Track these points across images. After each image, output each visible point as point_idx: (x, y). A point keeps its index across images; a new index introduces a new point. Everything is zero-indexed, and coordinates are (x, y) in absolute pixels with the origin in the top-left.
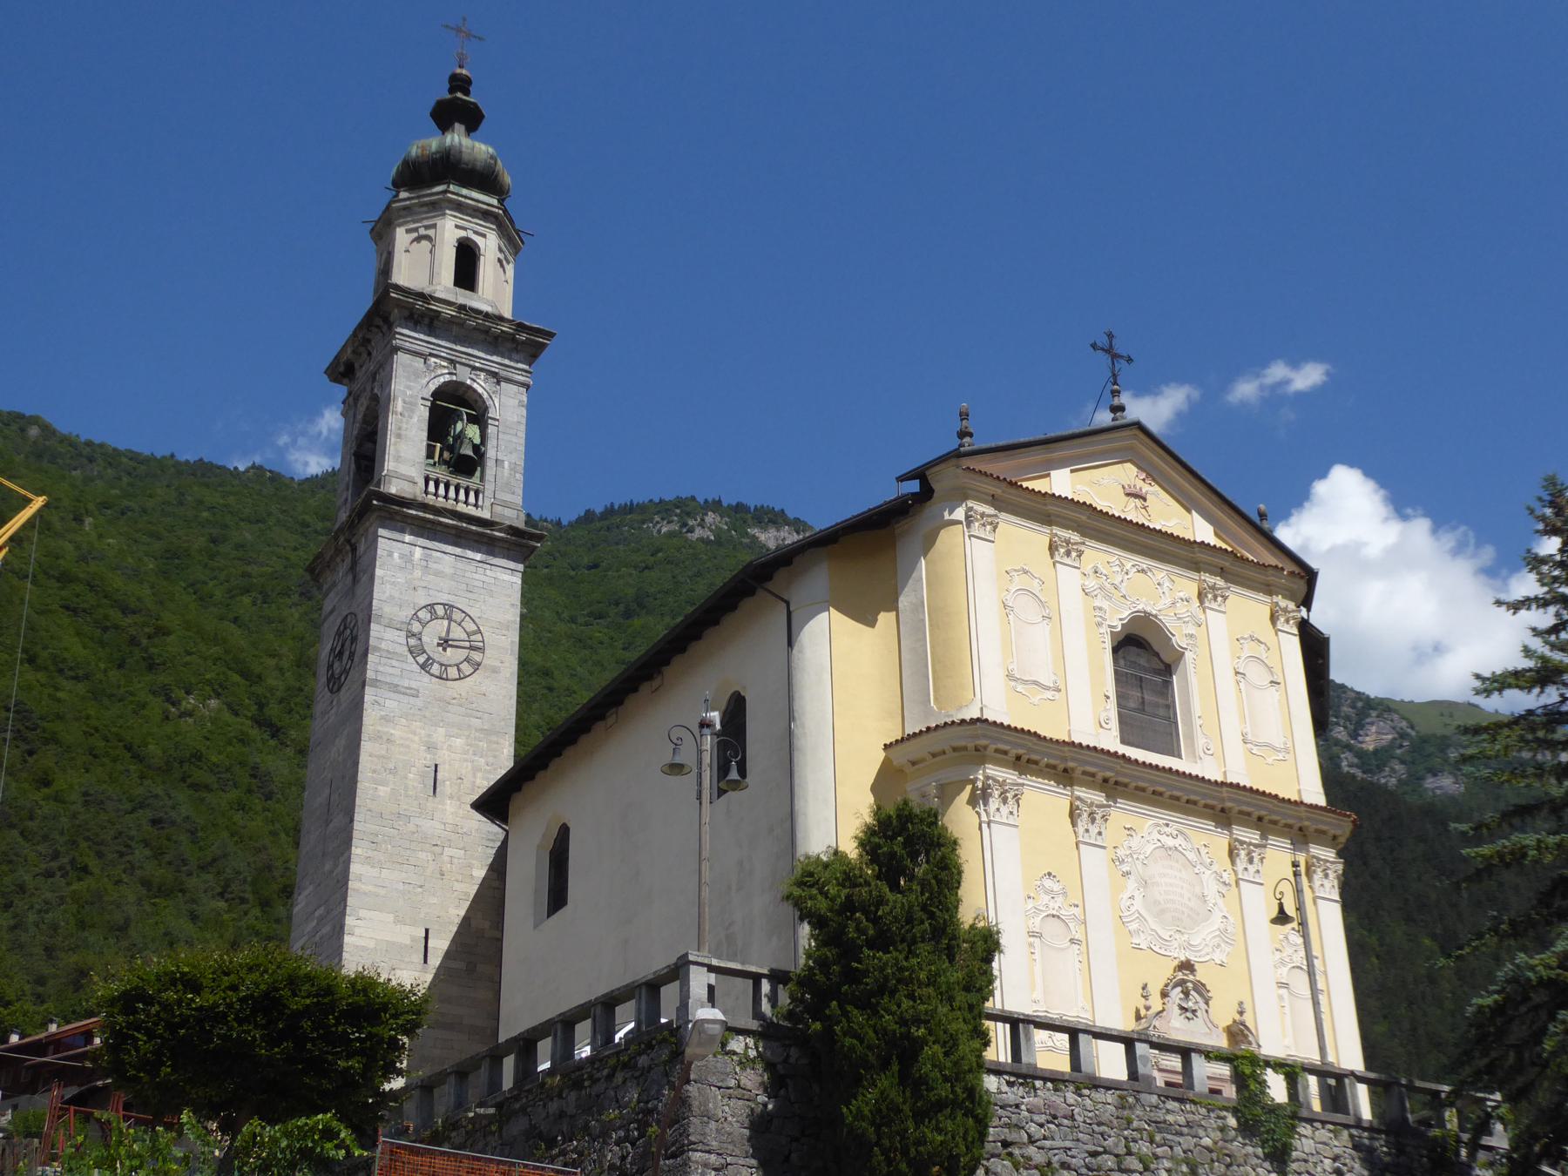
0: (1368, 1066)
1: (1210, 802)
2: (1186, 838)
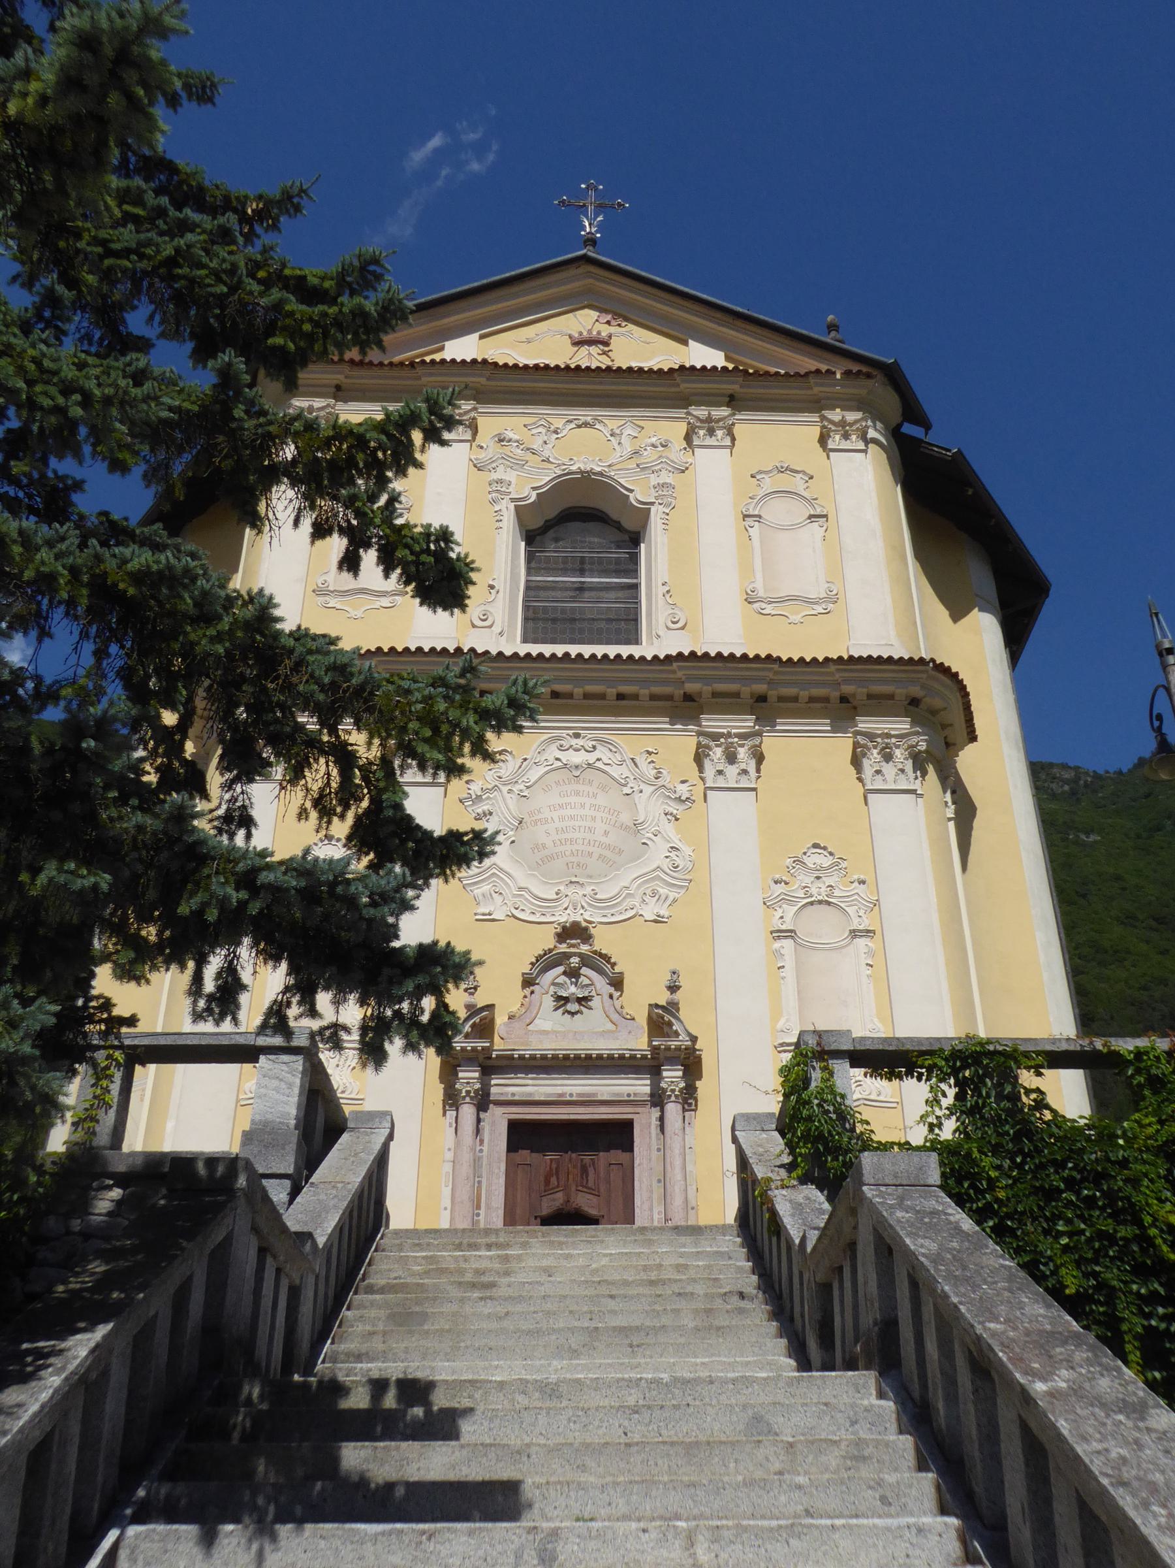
1: (657, 690)
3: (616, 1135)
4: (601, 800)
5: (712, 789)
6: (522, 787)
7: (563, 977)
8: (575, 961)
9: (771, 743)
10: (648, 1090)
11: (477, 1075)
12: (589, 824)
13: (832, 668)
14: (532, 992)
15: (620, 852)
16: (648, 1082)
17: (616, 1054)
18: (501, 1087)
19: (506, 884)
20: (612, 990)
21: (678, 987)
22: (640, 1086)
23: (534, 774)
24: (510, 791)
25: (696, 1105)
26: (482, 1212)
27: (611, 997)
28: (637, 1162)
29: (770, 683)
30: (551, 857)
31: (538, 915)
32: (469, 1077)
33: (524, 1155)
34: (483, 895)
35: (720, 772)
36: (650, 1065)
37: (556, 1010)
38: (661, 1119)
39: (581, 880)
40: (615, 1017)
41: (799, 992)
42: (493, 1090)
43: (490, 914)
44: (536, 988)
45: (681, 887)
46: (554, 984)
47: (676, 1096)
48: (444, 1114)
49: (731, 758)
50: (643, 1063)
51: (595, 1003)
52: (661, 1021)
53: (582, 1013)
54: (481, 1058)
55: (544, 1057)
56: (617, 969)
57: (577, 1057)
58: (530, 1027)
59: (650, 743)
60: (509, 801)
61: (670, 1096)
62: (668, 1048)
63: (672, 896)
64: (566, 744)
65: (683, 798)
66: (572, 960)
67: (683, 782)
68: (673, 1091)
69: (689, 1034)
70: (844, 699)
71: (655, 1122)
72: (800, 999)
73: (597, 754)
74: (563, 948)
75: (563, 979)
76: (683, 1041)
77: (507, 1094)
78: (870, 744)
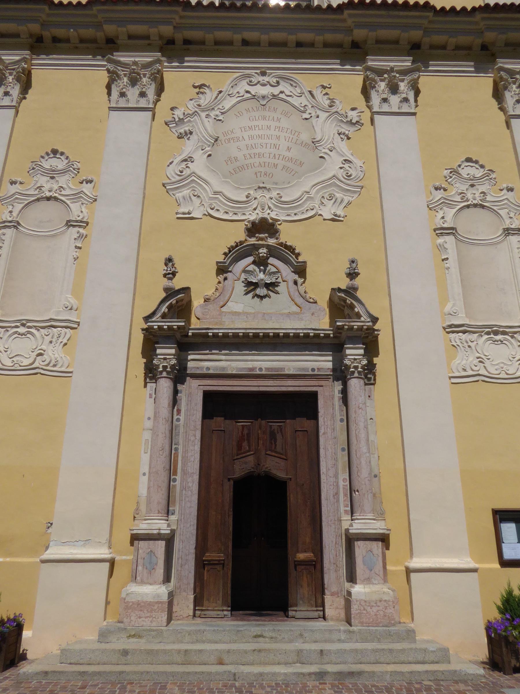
0: (330, 327)
1: (329, 37)
2: (293, 83)
3: (304, 405)
4: (284, 123)
5: (378, 113)
6: (217, 112)
7: (252, 266)
8: (263, 251)
9: (426, 81)
10: (330, 365)
11: (173, 351)
12: (274, 142)
13: (478, 16)
14: (225, 279)
15: (301, 164)
16: (330, 358)
17: (302, 333)
18: (196, 362)
19: (204, 189)
20: (296, 277)
21: (357, 274)
22: (324, 362)
23: (228, 103)
24: (208, 116)
25: (375, 380)
26: (178, 478)
27: (296, 283)
28: (322, 431)
29: (427, 32)
30: (242, 168)
31: (231, 214)
32: (166, 353)
33: (219, 422)
34: (184, 198)
35: (385, 100)
36: (333, 343)
37: (246, 294)
38: (344, 392)
39: (268, 186)
40: (300, 300)
41: (462, 281)
42: (190, 364)
43: (189, 213)
44: (229, 275)
45: (355, 192)
46: (244, 271)
47: (359, 373)
48: (145, 386)
49: (394, 89)
50: (325, 341)
51: (282, 288)
52: (342, 303)
53: (269, 297)
54: (178, 336)
55: (236, 335)
56: (301, 259)
57: (266, 335)
58: (223, 309)
59: (325, 80)
60: (207, 124)
61: (353, 373)
62: (351, 328)
63: (346, 199)
64: (254, 80)
65: (354, 121)
66: (261, 251)
67: (353, 109)
68: (356, 367)
69: (371, 316)
70: (484, 47)
71: (337, 395)
72: (463, 286)
73: (280, 88)
74: (252, 241)
75: (252, 267)
76: (365, 321)
77: (202, 368)
78: (510, 80)
